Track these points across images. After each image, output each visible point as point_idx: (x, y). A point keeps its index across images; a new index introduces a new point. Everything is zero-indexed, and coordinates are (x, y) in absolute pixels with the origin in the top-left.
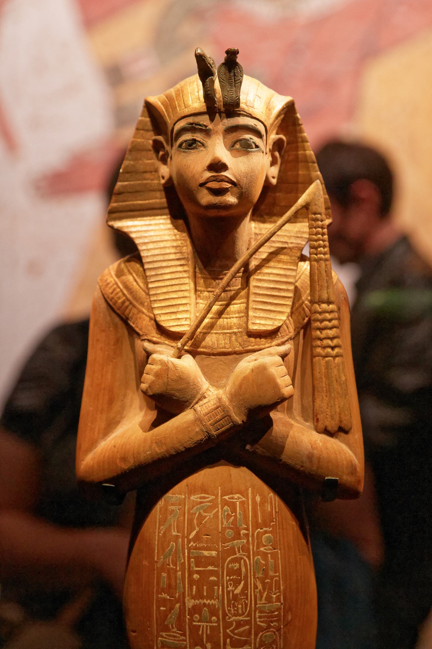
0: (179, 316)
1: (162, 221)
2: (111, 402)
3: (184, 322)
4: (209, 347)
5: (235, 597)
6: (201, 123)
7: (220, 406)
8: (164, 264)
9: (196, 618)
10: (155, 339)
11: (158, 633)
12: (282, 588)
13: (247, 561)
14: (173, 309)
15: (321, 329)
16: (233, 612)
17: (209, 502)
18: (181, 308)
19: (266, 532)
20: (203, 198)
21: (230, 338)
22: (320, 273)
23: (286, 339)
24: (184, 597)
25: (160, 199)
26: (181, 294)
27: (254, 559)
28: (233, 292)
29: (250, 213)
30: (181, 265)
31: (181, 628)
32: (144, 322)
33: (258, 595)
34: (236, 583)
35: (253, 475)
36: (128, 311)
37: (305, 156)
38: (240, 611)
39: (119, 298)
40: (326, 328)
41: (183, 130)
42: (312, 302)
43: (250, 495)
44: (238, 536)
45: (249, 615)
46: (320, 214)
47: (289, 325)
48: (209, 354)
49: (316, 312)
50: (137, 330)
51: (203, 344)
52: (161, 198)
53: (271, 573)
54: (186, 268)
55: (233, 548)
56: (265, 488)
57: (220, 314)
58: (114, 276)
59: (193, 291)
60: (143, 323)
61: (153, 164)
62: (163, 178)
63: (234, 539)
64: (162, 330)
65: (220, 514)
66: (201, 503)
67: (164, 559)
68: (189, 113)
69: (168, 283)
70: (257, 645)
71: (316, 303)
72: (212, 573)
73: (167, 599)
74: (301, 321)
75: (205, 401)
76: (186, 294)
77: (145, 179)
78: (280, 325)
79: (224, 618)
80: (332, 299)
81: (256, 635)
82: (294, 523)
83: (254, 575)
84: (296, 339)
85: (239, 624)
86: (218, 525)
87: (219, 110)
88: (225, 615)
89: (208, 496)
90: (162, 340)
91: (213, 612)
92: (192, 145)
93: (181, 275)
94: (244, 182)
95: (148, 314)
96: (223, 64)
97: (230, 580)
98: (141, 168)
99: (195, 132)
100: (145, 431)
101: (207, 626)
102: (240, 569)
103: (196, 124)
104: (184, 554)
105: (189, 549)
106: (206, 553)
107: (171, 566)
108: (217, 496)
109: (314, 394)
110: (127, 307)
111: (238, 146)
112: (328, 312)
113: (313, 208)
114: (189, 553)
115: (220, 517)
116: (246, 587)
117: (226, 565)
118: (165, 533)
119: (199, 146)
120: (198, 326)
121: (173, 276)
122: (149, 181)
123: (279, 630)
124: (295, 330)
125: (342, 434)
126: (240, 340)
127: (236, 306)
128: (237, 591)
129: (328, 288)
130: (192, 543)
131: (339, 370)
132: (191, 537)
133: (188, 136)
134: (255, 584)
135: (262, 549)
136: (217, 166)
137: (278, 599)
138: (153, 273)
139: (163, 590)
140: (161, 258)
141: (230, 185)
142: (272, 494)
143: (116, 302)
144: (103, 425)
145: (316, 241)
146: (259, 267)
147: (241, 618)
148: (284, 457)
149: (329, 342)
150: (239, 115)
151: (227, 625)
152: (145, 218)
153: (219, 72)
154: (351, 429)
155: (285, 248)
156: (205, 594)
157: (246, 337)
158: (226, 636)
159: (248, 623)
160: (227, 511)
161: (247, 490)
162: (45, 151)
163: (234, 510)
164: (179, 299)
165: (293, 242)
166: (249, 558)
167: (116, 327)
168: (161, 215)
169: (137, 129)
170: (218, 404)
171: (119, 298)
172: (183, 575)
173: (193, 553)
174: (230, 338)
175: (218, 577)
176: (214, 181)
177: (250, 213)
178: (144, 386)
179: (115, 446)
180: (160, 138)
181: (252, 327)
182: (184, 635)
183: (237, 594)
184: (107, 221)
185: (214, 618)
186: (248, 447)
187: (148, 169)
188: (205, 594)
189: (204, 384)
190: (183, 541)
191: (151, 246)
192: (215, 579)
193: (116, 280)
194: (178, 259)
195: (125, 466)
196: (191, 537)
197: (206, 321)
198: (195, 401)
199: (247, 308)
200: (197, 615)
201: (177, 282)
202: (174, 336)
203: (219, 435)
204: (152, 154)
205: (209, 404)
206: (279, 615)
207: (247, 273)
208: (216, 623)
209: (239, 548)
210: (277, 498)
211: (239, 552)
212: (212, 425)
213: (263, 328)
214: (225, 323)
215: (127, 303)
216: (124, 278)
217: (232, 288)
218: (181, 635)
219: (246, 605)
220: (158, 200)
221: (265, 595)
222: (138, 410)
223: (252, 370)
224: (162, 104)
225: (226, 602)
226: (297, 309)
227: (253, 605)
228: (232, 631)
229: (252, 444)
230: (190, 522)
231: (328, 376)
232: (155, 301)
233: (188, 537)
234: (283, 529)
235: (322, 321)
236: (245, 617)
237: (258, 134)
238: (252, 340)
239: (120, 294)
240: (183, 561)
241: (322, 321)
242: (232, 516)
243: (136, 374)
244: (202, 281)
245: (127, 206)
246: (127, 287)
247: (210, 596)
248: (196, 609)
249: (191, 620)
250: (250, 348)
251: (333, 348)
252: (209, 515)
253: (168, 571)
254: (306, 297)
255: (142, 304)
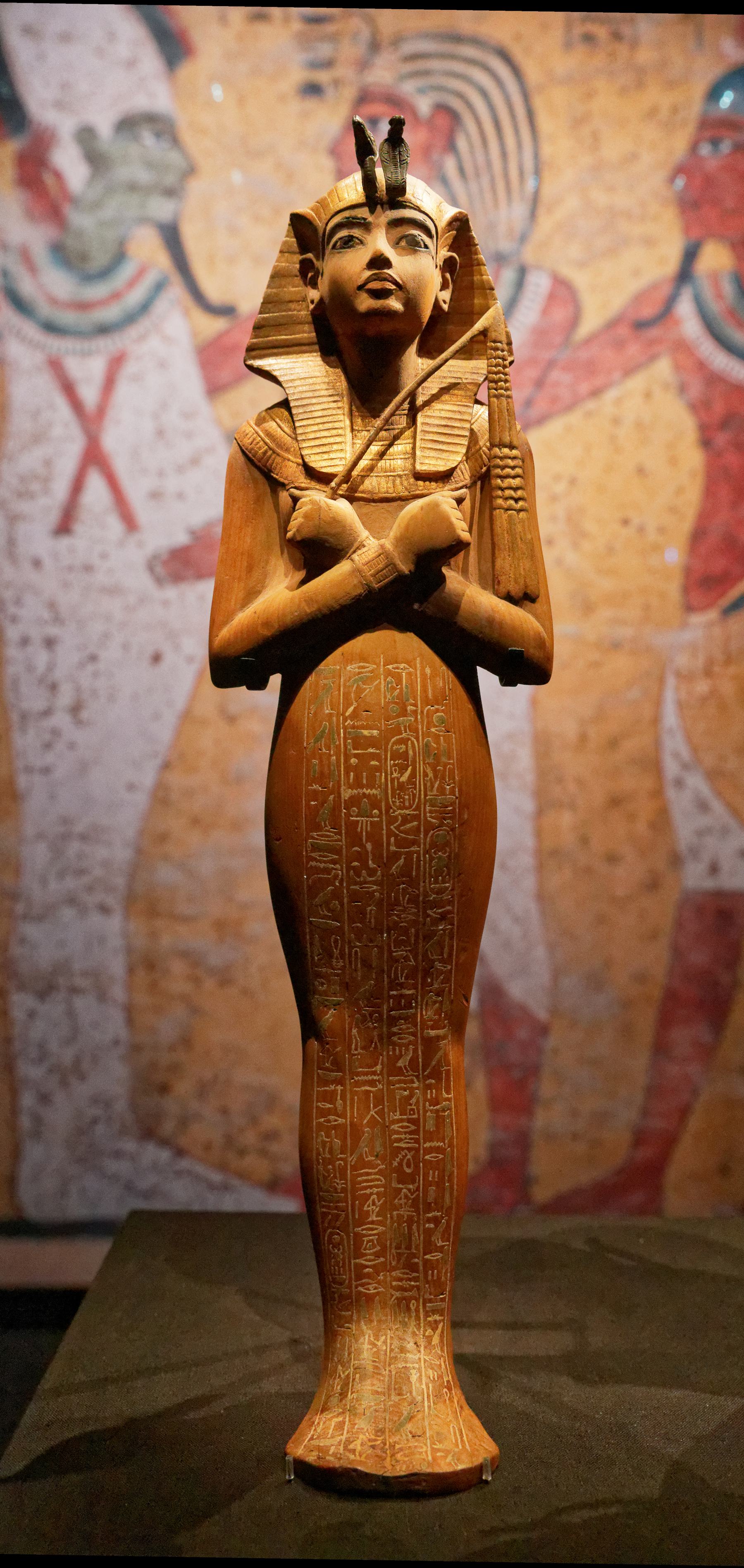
0: (332, 455)
1: (310, 358)
2: (250, 569)
3: (337, 462)
4: (369, 492)
5: (401, 786)
6: (359, 216)
7: (383, 552)
8: (314, 401)
9: (354, 811)
10: (303, 485)
11: (308, 834)
12: (457, 778)
13: (416, 742)
14: (325, 449)
15: (503, 477)
16: (398, 804)
17: (369, 672)
18: (335, 447)
19: (437, 711)
20: (362, 303)
21: (394, 481)
22: (500, 411)
23: (460, 484)
24: (339, 787)
25: (307, 333)
26: (334, 432)
27: (423, 740)
28: (397, 431)
29: (416, 341)
30: (334, 402)
31: (335, 826)
32: (291, 470)
33: (429, 784)
34: (402, 769)
35: (422, 643)
36: (270, 461)
37: (482, 281)
38: (407, 804)
39: (260, 448)
40: (507, 466)
41: (339, 226)
42: (493, 445)
43: (418, 665)
44: (404, 713)
45: (418, 808)
46: (500, 342)
47: (464, 471)
48: (368, 501)
49: (496, 457)
50: (282, 480)
51: (361, 488)
52: (310, 332)
53: (444, 759)
54: (340, 404)
55: (398, 726)
56: (437, 661)
57: (382, 455)
58: (254, 426)
59: (348, 430)
60: (290, 471)
61: (299, 292)
62: (312, 302)
63: (398, 716)
64: (311, 473)
65: (382, 686)
66: (359, 673)
67: (315, 743)
68: (345, 206)
69: (318, 420)
70: (428, 846)
71: (496, 446)
72: (373, 756)
73: (319, 791)
74: (478, 469)
75: (364, 550)
76: (340, 432)
77: (290, 310)
78: (453, 466)
79: (387, 811)
80: (515, 443)
81: (426, 835)
82: (470, 706)
83: (424, 761)
84: (473, 489)
85: (406, 820)
86: (380, 699)
87: (381, 200)
88: (388, 808)
89: (367, 665)
90: (313, 484)
91: (375, 803)
92: (348, 243)
93: (334, 412)
94: (410, 285)
95: (294, 460)
96: (386, 140)
97: (395, 765)
98: (287, 297)
99: (352, 225)
100: (292, 590)
101: (367, 821)
102: (406, 752)
103: (353, 218)
104: (339, 734)
105: (345, 728)
106: (366, 732)
107: (324, 750)
108: (378, 665)
109: (493, 554)
110: (270, 456)
111: (403, 243)
112: (510, 458)
113: (493, 335)
114: (344, 734)
115: (383, 690)
116: (413, 775)
117: (389, 747)
118: (315, 713)
119: (358, 244)
120: (355, 464)
121: (325, 413)
122: (295, 312)
123: (453, 830)
124: (471, 477)
125: (528, 603)
126: (405, 483)
127: (402, 447)
128: (404, 779)
129: (510, 429)
130: (349, 721)
131: (523, 527)
132: (347, 714)
133: (344, 233)
134: (424, 771)
135: (433, 730)
136: (379, 262)
137: (452, 792)
138: (301, 410)
139: (314, 781)
140: (310, 394)
141: (394, 287)
142: (444, 668)
143: (256, 452)
144: (241, 595)
145: (496, 373)
146: (427, 403)
147: (407, 812)
148: (460, 620)
149: (512, 493)
150: (405, 207)
151: (390, 822)
152: (291, 356)
153: (381, 150)
154: (538, 597)
155: (459, 384)
156: (365, 782)
157: (412, 480)
158: (390, 833)
159: (416, 817)
160: (392, 682)
161: (415, 659)
162: (166, 530)
163: (399, 681)
164: (333, 437)
165: (467, 378)
166: (417, 739)
167: (255, 481)
168: (311, 352)
169: (281, 252)
170: (381, 551)
171: (260, 448)
172: (338, 760)
173: (349, 733)
174: (394, 481)
175: (380, 761)
176: (375, 280)
177: (416, 341)
178: (289, 535)
179: (255, 613)
180: (310, 255)
181: (419, 467)
182: (340, 834)
183: (403, 782)
184: (245, 361)
185: (375, 811)
186: (416, 606)
187: (294, 298)
188: (365, 782)
189: (363, 534)
190: (338, 720)
191: (298, 383)
192: (377, 763)
193: (256, 428)
194: (330, 396)
195: (267, 633)
196: (347, 714)
197: (363, 464)
198: (352, 550)
199: (414, 448)
200: (355, 809)
201: (330, 419)
202: (323, 478)
203: (380, 589)
204: (298, 280)
205: (369, 552)
206: (454, 811)
207: (413, 412)
208: (378, 817)
209: (405, 727)
210: (450, 673)
211: (406, 732)
212: (374, 575)
213: (433, 469)
214: (388, 464)
215: (270, 452)
216: (266, 425)
217: (395, 427)
218: (336, 834)
219: (414, 795)
220: (305, 335)
221: (436, 786)
222: (283, 576)
223: (422, 508)
224: (312, 210)
225: (390, 791)
226: (473, 455)
227: (422, 797)
228: (397, 828)
229: (421, 603)
230: (347, 695)
231: (511, 531)
232: (304, 440)
233: (343, 714)
234: (457, 709)
235: (503, 468)
236: (414, 810)
237: (430, 235)
238: (421, 483)
239: (261, 443)
240: (337, 743)
241: (503, 468)
242: (396, 689)
243: (280, 532)
244: (359, 420)
245: (269, 341)
246: (268, 434)
247: (371, 786)
248: (354, 801)
249: (348, 815)
250: (418, 492)
251: (516, 500)
252: (368, 689)
253: (321, 756)
254: (483, 441)
255: (287, 450)
